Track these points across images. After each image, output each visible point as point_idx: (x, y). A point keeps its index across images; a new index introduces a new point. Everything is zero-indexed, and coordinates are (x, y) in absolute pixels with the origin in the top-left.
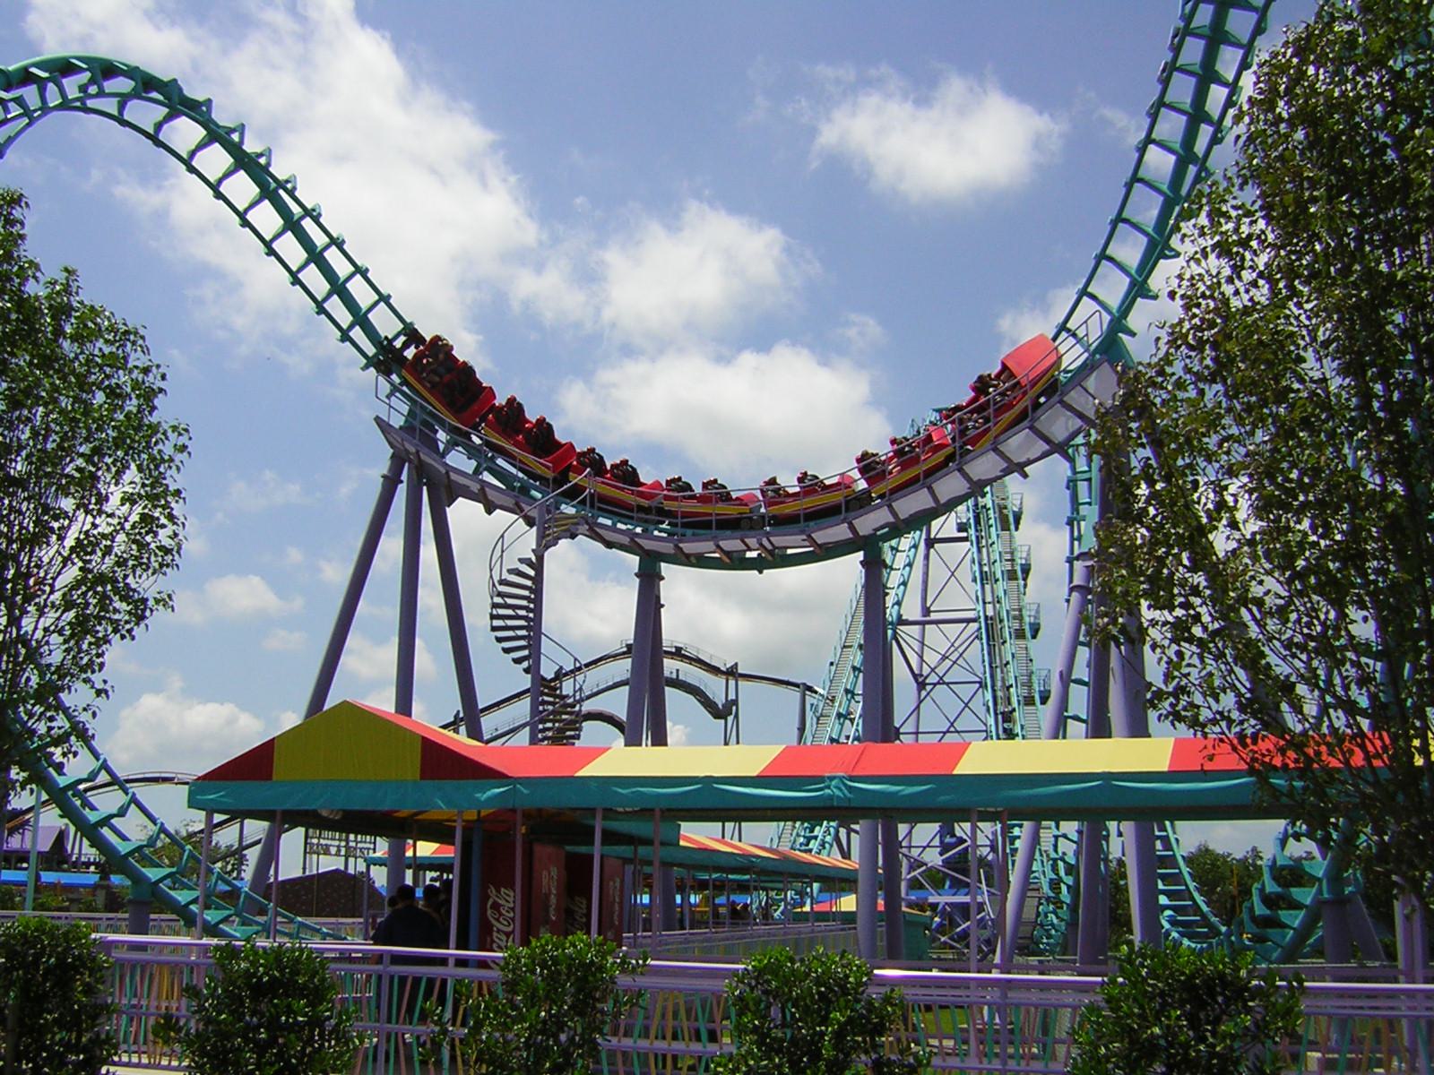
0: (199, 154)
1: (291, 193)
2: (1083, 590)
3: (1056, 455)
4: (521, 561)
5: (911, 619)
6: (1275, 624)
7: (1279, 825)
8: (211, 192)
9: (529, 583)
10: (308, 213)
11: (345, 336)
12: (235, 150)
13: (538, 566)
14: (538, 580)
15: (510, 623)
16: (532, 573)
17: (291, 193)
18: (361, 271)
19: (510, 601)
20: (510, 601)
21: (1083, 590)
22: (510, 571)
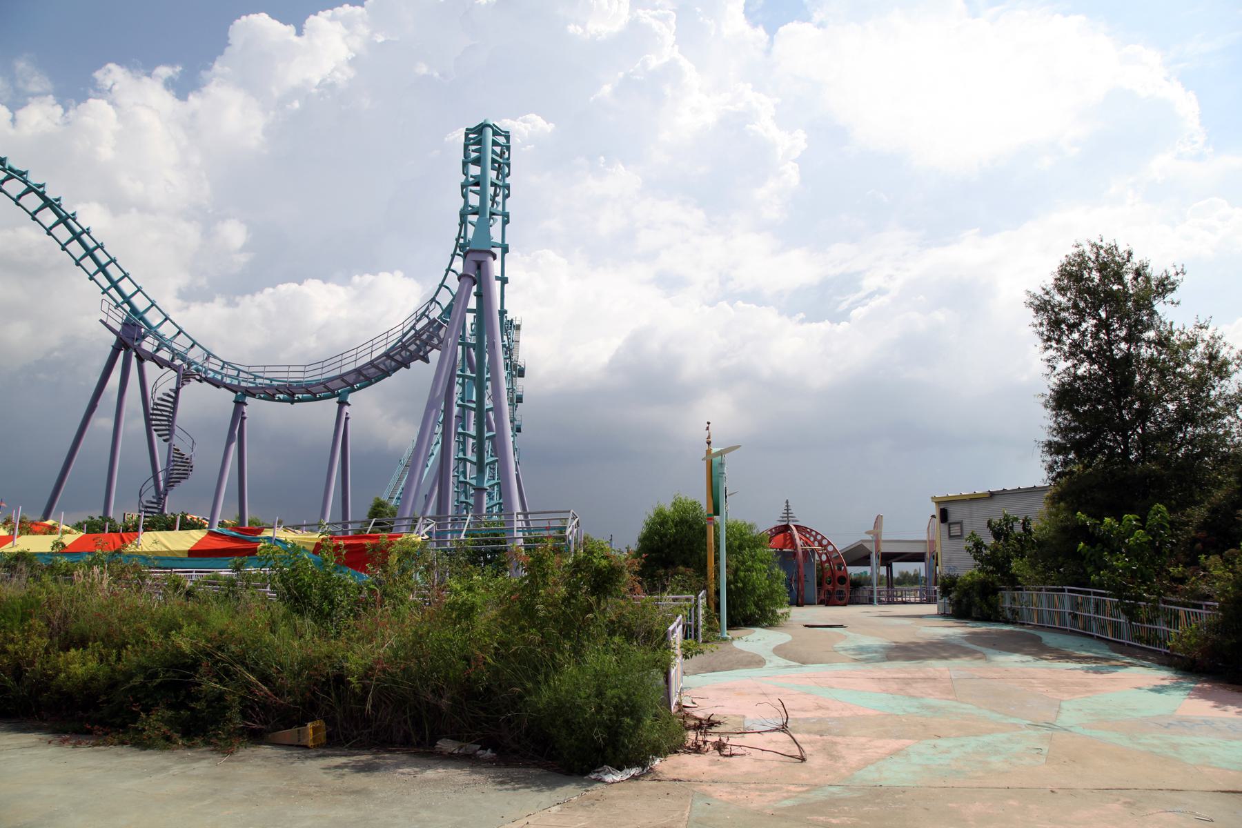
0: (23, 197)
1: (74, 220)
2: (246, 747)
3: (435, 350)
4: (164, 394)
5: (237, 513)
6: (538, 640)
7: (492, 194)
8: (30, 217)
9: (171, 400)
10: (84, 231)
11: (105, 291)
12: (42, 195)
13: (177, 391)
14: (176, 399)
15: (159, 417)
16: (173, 395)
17: (74, 220)
18: (113, 261)
19: (159, 407)
20: (159, 407)
21: (246, 747)
22: (159, 399)
